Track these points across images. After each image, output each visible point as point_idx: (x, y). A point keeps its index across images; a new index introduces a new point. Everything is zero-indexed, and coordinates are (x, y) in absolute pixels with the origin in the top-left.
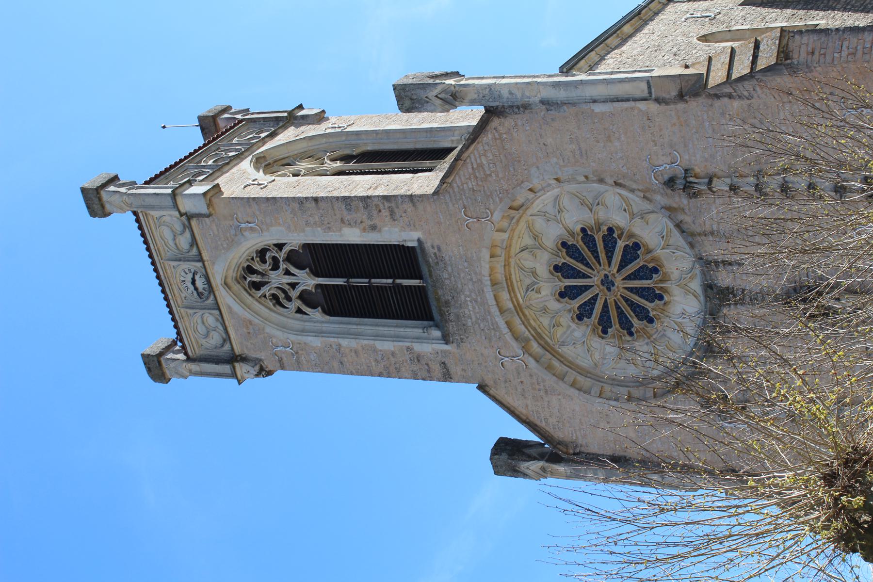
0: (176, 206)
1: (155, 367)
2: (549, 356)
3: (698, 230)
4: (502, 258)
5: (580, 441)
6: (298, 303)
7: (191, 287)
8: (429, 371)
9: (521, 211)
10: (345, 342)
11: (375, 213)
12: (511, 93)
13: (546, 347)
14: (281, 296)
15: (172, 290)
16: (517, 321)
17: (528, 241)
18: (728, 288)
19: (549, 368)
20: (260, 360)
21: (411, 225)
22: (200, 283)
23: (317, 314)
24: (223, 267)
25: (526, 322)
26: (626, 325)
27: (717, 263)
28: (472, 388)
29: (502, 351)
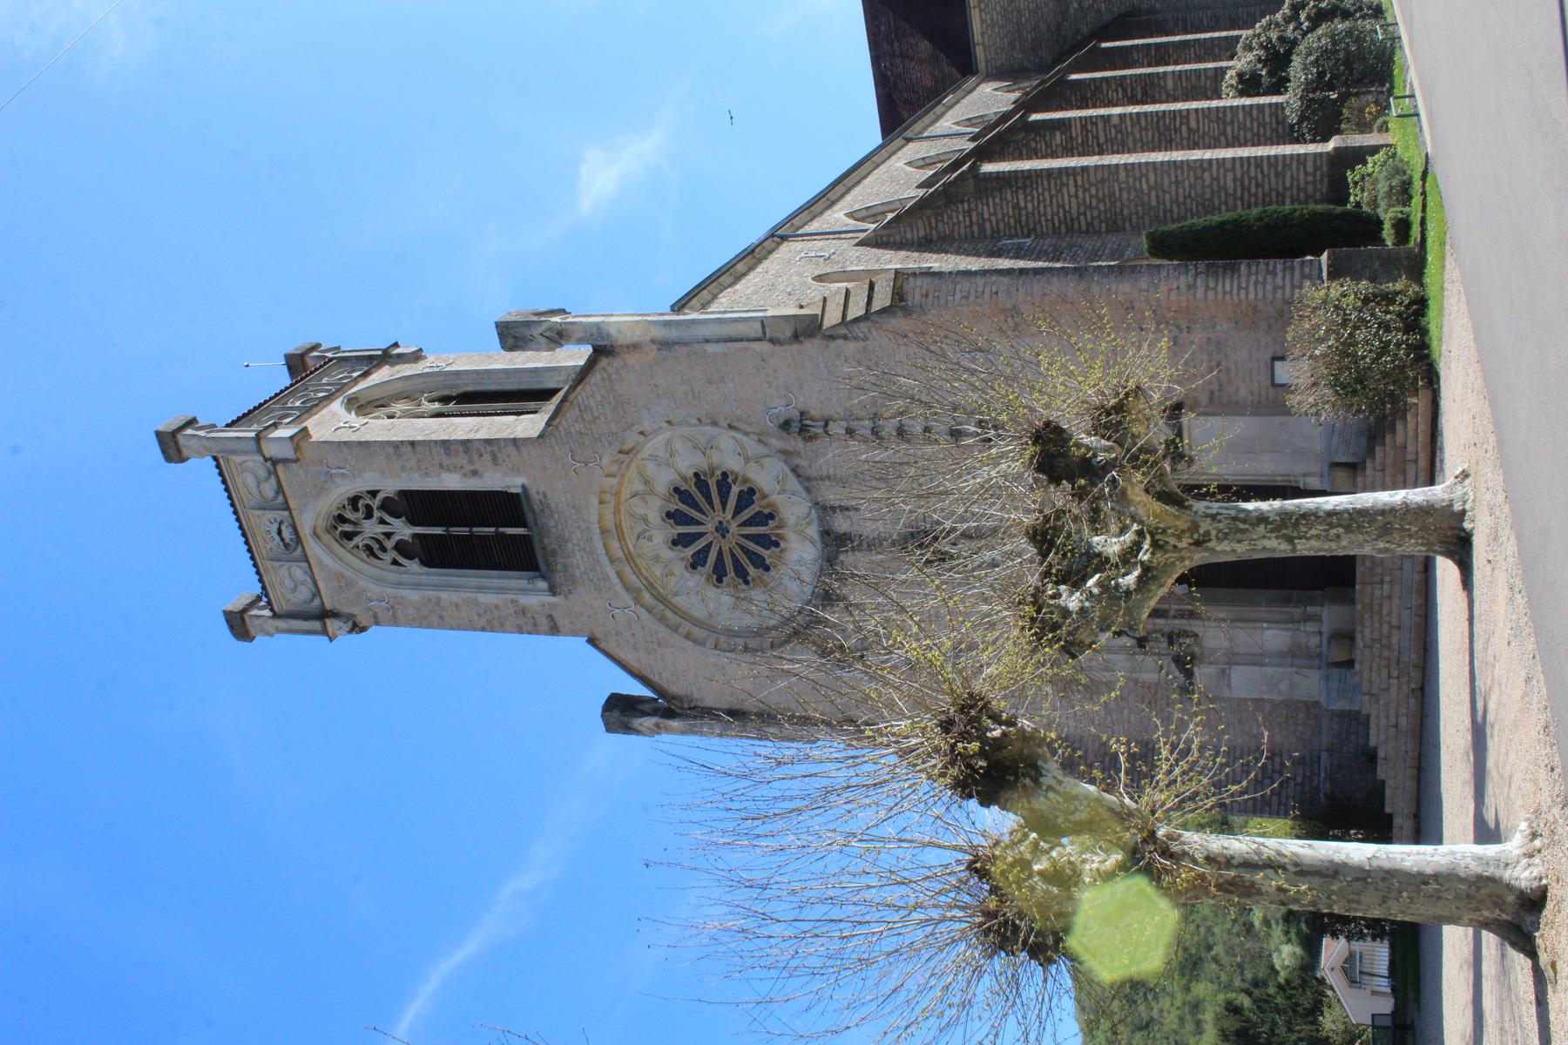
0: (260, 451)
2: (662, 607)
3: (815, 474)
7: (277, 538)
10: (444, 595)
11: (476, 457)
13: (659, 598)
14: (376, 546)
15: (256, 541)
16: (628, 571)
17: (638, 486)
19: (662, 619)
21: (515, 470)
22: (287, 533)
23: (414, 566)
24: (311, 517)
26: (742, 574)
27: (833, 509)
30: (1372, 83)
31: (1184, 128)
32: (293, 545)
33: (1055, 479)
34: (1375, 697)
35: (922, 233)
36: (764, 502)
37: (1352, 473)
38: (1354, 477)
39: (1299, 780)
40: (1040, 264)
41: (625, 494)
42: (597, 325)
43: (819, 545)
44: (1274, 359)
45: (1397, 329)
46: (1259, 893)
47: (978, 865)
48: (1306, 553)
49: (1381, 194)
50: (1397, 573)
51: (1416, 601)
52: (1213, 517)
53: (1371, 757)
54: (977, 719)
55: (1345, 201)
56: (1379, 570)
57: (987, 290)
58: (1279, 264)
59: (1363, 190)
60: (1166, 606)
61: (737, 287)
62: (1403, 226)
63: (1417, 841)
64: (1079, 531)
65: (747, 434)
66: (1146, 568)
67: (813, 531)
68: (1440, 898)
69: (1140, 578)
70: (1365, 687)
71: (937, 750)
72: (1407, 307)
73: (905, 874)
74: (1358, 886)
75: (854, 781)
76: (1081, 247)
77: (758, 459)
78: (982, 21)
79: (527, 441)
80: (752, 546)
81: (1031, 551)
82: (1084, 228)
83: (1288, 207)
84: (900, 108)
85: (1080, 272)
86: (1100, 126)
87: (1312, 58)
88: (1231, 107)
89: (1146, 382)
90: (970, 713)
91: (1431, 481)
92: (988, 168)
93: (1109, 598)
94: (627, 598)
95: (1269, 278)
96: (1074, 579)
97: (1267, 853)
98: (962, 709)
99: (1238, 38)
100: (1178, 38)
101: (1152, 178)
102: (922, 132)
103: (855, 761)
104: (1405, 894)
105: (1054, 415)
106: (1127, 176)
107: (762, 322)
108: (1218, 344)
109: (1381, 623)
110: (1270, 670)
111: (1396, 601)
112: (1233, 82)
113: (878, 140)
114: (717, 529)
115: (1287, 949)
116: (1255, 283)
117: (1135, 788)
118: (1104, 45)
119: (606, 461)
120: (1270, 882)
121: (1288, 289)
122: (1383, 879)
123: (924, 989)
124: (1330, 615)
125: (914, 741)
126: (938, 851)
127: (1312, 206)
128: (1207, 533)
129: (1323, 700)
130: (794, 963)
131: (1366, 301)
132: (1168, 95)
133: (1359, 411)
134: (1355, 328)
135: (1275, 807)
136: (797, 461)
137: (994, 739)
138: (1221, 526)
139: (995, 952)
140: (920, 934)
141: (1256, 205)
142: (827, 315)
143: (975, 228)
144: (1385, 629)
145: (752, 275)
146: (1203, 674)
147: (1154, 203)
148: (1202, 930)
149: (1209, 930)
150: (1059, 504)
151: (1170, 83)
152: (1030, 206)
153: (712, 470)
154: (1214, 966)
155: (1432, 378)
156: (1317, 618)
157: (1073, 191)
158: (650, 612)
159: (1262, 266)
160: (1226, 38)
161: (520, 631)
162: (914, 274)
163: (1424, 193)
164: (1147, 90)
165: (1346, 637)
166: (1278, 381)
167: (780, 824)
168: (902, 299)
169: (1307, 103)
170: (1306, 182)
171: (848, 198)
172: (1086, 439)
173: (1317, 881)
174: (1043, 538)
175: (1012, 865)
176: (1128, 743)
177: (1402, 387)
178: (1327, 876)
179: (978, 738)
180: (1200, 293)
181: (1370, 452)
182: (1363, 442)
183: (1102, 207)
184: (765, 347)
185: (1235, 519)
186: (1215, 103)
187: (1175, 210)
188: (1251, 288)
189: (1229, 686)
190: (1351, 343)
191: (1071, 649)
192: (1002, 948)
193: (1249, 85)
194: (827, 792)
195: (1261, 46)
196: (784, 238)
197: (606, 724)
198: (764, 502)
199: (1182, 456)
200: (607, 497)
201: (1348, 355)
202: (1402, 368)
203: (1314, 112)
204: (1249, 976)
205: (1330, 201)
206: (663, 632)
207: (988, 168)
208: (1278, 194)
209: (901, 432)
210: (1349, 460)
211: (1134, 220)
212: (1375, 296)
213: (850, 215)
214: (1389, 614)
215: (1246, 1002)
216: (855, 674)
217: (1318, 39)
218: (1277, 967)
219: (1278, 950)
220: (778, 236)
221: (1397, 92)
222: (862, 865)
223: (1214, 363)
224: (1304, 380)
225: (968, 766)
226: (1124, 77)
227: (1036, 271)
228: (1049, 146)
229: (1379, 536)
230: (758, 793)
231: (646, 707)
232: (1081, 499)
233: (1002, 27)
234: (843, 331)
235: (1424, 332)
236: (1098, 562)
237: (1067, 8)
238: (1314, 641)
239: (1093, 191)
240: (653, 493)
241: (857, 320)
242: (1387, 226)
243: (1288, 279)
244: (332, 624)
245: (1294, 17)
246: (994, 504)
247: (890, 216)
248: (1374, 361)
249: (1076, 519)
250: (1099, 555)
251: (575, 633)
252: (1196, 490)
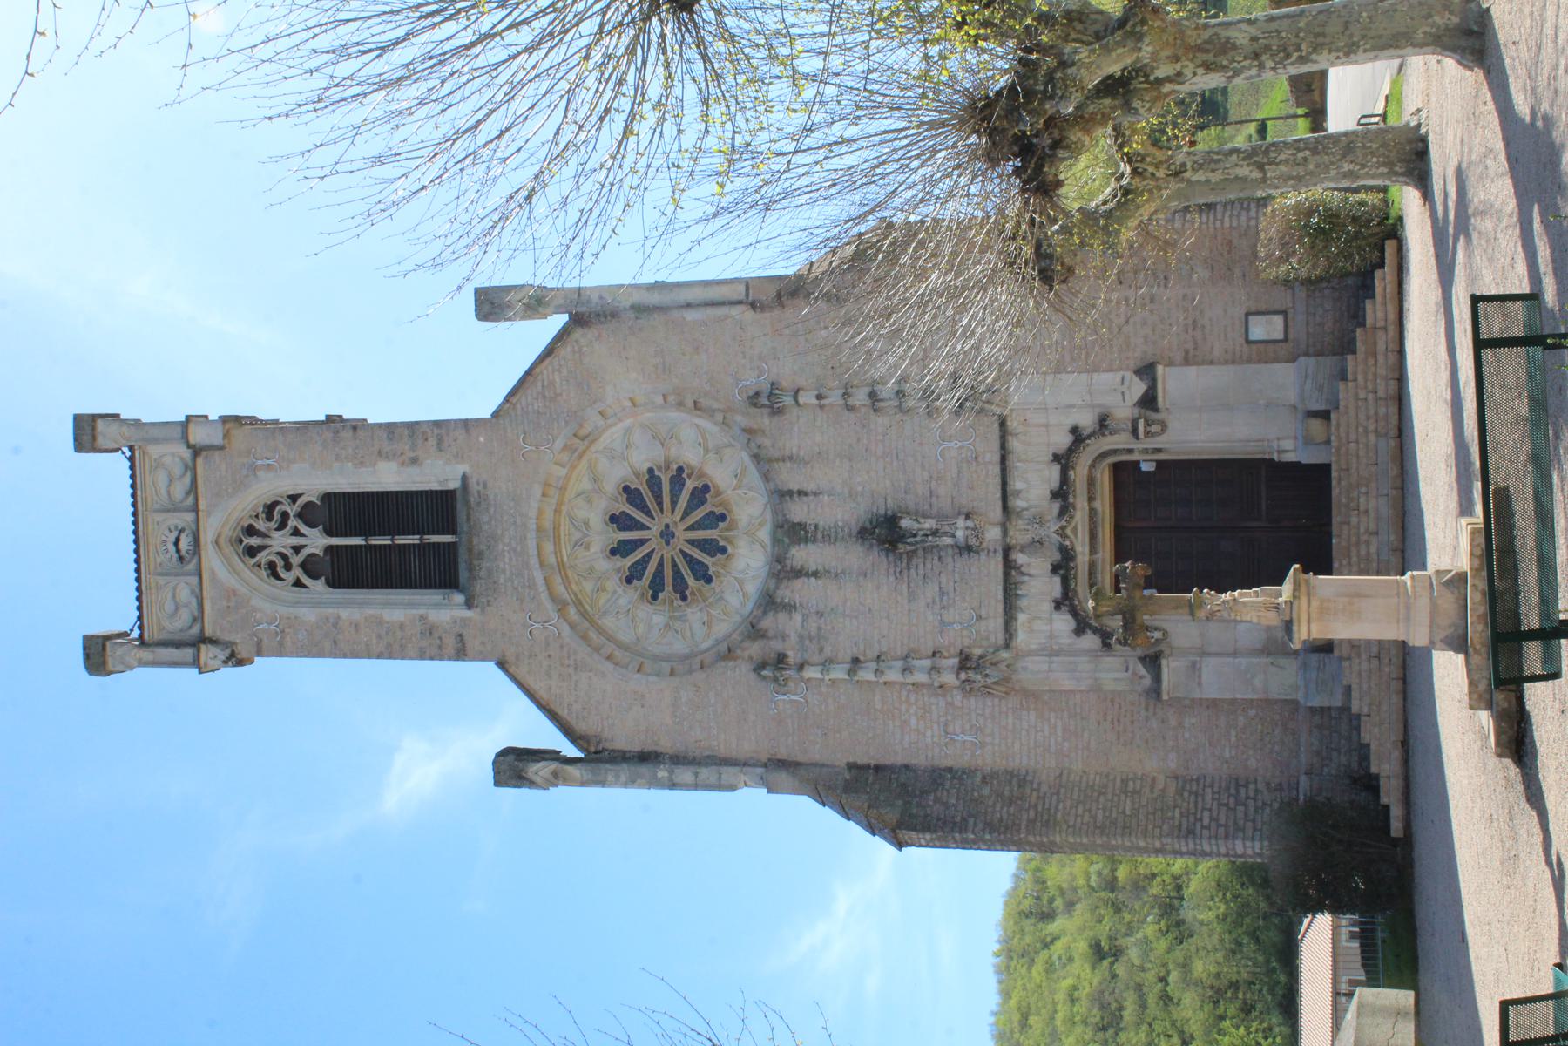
1: (98, 654)
2: (586, 624)
3: (777, 454)
5: (606, 734)
6: (297, 572)
7: (172, 549)
8: (440, 648)
10: (345, 614)
11: (420, 442)
12: (601, 298)
13: (584, 614)
14: (280, 563)
15: (147, 551)
17: (586, 485)
18: (800, 524)
19: (585, 638)
20: (235, 643)
21: (459, 457)
23: (318, 586)
24: (218, 522)
25: (567, 583)
26: (681, 588)
27: (790, 493)
28: (491, 666)
32: (188, 555)
79: (479, 422)
95: (1244, 213)
110: (1243, 662)
128: (1183, 165)
129: (1300, 696)
135: (1249, 832)
161: (422, 655)
184: (749, 315)
189: (1200, 684)
244: (207, 652)
251: (483, 657)
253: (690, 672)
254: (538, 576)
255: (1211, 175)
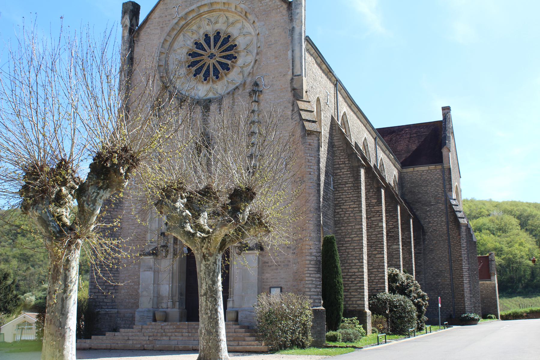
2: (178, 29)
3: (235, 96)
4: (223, 8)
5: (139, 43)
9: (244, 17)
12: (298, 13)
13: (182, 28)
16: (194, 14)
17: (231, 20)
18: (209, 109)
19: (173, 29)
25: (194, 18)
26: (193, 64)
29: (180, 7)
30: (392, 327)
31: (376, 252)
33: (231, 197)
34: (141, 331)
35: (336, 144)
36: (224, 75)
37: (234, 319)
38: (232, 321)
39: (105, 300)
40: (322, 193)
41: (228, 14)
42: (301, 4)
43: (205, 98)
44: (281, 288)
45: (292, 337)
46: (54, 283)
47: (63, 163)
48: (200, 301)
49: (347, 330)
50: (192, 339)
51: (181, 346)
52: (215, 263)
53: (115, 330)
54: (128, 162)
55: (345, 316)
56: (194, 331)
57: (311, 170)
58: (320, 290)
59: (349, 323)
60: (178, 243)
61: (316, 65)
62: (334, 339)
63: (78, 349)
64: (209, 207)
65: (253, 68)
66: (193, 235)
67: (211, 95)
68: (53, 357)
69: (190, 232)
70: (145, 326)
71: (115, 146)
72: (301, 341)
73: (59, 131)
74: (58, 324)
75: (100, 109)
76: (329, 209)
77: (242, 72)
78: (423, 171)
80: (205, 69)
81: (201, 187)
82: (337, 211)
83: (343, 293)
84: (389, 136)
85: (318, 209)
86: (379, 218)
87: (402, 303)
88: (384, 271)
89: (272, 235)
90: (131, 161)
91: (229, 352)
92: (362, 171)
93: (181, 220)
94: (182, 14)
95: (314, 286)
96: (189, 205)
97: (71, 286)
98: (132, 156)
99: (412, 274)
100: (413, 250)
101: (356, 239)
102: (378, 145)
103: (109, 109)
104: (54, 343)
105: (258, 196)
106: (357, 229)
107: (301, 75)
108: (288, 265)
109: (172, 332)
110: (151, 287)
111: (180, 338)
112: (394, 272)
113: (376, 127)
114: (212, 54)
115: (33, 298)
116: (312, 280)
117: (98, 230)
118: (411, 220)
119: (242, 6)
120: (58, 288)
121: (309, 293)
122: (61, 334)
123: (8, 140)
124: (175, 312)
125: (118, 136)
126: (70, 146)
127: (343, 303)
128: (208, 260)
129: (140, 309)
130: (17, 82)
131: (304, 324)
132: (390, 246)
133: (259, 322)
134: (293, 320)
136: (241, 89)
137: (119, 170)
138: (211, 266)
139: (24, 170)
140: (33, 139)
141: (344, 281)
142: (303, 103)
143: (338, 166)
144: (169, 334)
145: (321, 71)
146: (150, 259)
147: (346, 239)
148: (41, 263)
149: (41, 266)
150: (220, 198)
151: (395, 247)
152: (346, 189)
153: (238, 52)
154: (25, 268)
155: (272, 351)
156: (174, 306)
157: (352, 206)
158: (176, 24)
159: (319, 283)
160: (412, 270)
162: (319, 140)
163: (347, 347)
164: (392, 237)
165: (166, 319)
166: (272, 289)
167: (80, 75)
168: (308, 134)
169: (385, 302)
170: (353, 301)
171: (352, 113)
172: (248, 210)
173: (59, 306)
174: (207, 192)
175: (64, 178)
176: (117, 226)
177: (269, 339)
178: (62, 310)
179: (120, 163)
180: (308, 258)
181: (242, 327)
182: (247, 324)
183: (345, 218)
184: (289, 77)
185: (214, 271)
186: (386, 265)
187: (343, 248)
188: (310, 279)
189: (145, 271)
190: (287, 318)
191: (159, 203)
192: (27, 174)
193: (393, 278)
194: (95, 98)
195: (408, 283)
196: (336, 85)
197: (126, 3)
198: (224, 75)
199: (241, 250)
200: (226, 6)
201: (282, 317)
202: (276, 339)
203: (381, 304)
204: (21, 283)
205: (345, 310)
206: (167, 29)
207: (362, 171)
208: (349, 290)
209: (253, 133)
210: (239, 319)
211: (339, 231)
212: (306, 328)
213: (345, 114)
214: (176, 336)
215: (9, 282)
216: (148, 109)
217: (410, 306)
218: (25, 295)
219: (33, 295)
220: (337, 83)
221: (387, 336)
222: (63, 113)
223: (279, 263)
224: (272, 300)
225: (107, 159)
226: (398, 228)
227: (319, 191)
228: (371, 197)
229: (207, 330)
230: (94, 66)
231: (134, 21)
232: (222, 207)
233: (420, 179)
234: (296, 109)
235: (291, 348)
236: (196, 216)
237: (427, 206)
238: (164, 306)
239: (352, 215)
240: (228, 26)
241: (300, 115)
242: (334, 333)
243: (313, 293)
245: (419, 296)
246: (221, 172)
247: (344, 131)
248: (280, 328)
249: (214, 205)
250: (199, 215)
252: (227, 255)
253: (159, 73)
254: (194, 7)
255: (203, 272)
